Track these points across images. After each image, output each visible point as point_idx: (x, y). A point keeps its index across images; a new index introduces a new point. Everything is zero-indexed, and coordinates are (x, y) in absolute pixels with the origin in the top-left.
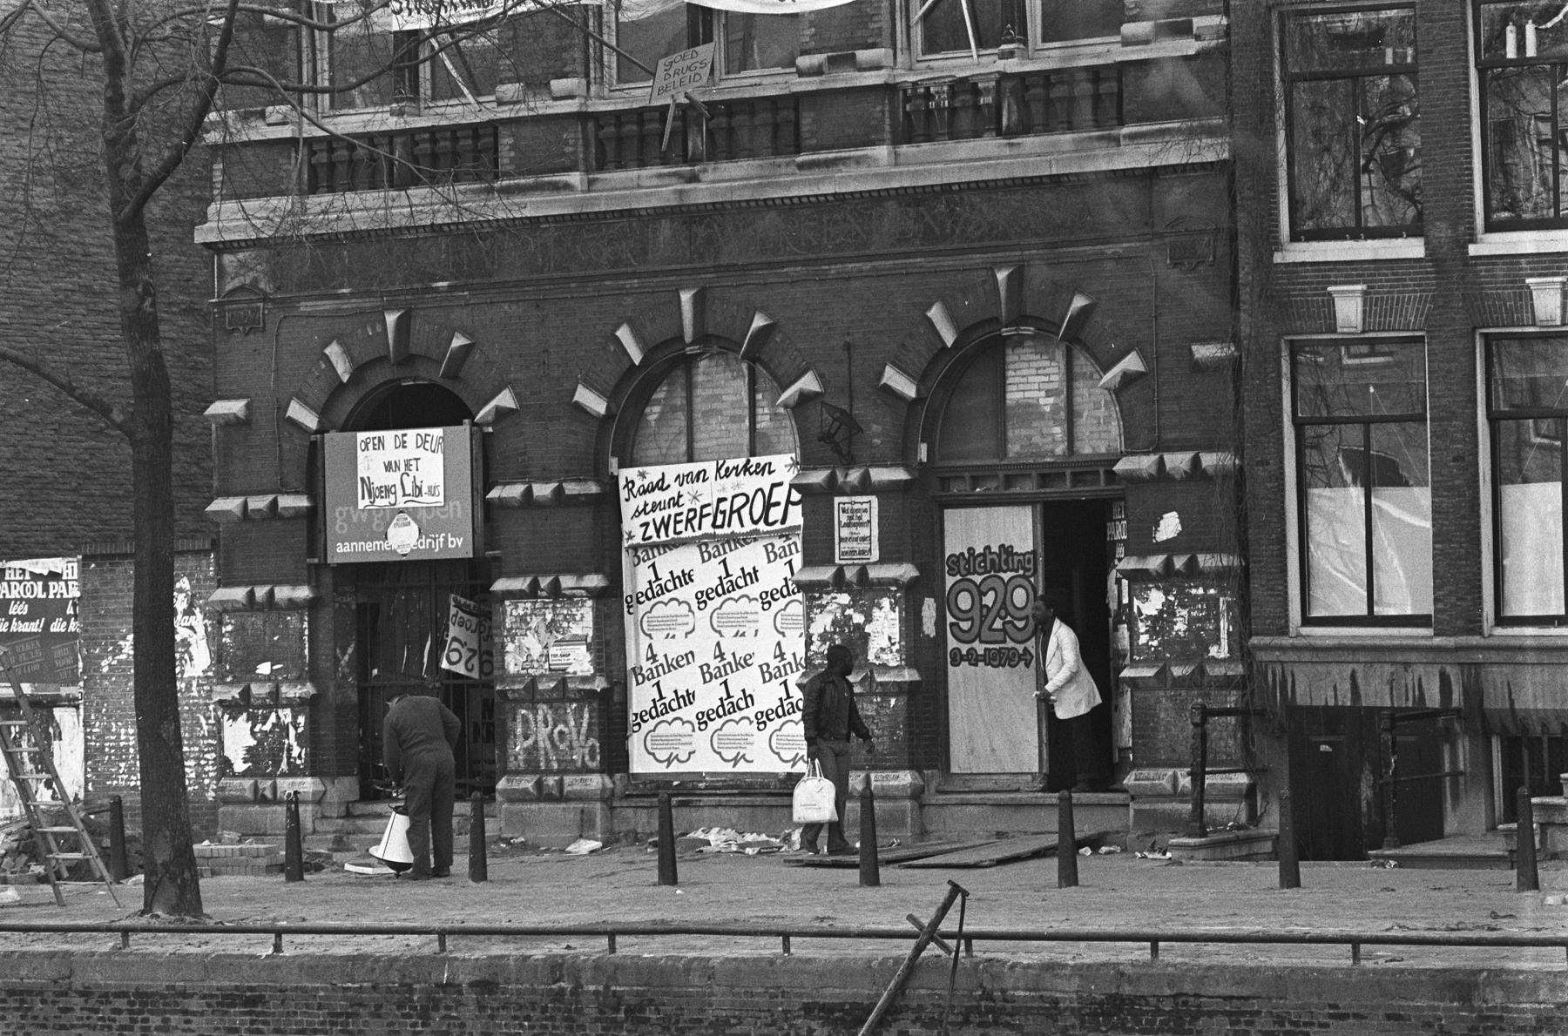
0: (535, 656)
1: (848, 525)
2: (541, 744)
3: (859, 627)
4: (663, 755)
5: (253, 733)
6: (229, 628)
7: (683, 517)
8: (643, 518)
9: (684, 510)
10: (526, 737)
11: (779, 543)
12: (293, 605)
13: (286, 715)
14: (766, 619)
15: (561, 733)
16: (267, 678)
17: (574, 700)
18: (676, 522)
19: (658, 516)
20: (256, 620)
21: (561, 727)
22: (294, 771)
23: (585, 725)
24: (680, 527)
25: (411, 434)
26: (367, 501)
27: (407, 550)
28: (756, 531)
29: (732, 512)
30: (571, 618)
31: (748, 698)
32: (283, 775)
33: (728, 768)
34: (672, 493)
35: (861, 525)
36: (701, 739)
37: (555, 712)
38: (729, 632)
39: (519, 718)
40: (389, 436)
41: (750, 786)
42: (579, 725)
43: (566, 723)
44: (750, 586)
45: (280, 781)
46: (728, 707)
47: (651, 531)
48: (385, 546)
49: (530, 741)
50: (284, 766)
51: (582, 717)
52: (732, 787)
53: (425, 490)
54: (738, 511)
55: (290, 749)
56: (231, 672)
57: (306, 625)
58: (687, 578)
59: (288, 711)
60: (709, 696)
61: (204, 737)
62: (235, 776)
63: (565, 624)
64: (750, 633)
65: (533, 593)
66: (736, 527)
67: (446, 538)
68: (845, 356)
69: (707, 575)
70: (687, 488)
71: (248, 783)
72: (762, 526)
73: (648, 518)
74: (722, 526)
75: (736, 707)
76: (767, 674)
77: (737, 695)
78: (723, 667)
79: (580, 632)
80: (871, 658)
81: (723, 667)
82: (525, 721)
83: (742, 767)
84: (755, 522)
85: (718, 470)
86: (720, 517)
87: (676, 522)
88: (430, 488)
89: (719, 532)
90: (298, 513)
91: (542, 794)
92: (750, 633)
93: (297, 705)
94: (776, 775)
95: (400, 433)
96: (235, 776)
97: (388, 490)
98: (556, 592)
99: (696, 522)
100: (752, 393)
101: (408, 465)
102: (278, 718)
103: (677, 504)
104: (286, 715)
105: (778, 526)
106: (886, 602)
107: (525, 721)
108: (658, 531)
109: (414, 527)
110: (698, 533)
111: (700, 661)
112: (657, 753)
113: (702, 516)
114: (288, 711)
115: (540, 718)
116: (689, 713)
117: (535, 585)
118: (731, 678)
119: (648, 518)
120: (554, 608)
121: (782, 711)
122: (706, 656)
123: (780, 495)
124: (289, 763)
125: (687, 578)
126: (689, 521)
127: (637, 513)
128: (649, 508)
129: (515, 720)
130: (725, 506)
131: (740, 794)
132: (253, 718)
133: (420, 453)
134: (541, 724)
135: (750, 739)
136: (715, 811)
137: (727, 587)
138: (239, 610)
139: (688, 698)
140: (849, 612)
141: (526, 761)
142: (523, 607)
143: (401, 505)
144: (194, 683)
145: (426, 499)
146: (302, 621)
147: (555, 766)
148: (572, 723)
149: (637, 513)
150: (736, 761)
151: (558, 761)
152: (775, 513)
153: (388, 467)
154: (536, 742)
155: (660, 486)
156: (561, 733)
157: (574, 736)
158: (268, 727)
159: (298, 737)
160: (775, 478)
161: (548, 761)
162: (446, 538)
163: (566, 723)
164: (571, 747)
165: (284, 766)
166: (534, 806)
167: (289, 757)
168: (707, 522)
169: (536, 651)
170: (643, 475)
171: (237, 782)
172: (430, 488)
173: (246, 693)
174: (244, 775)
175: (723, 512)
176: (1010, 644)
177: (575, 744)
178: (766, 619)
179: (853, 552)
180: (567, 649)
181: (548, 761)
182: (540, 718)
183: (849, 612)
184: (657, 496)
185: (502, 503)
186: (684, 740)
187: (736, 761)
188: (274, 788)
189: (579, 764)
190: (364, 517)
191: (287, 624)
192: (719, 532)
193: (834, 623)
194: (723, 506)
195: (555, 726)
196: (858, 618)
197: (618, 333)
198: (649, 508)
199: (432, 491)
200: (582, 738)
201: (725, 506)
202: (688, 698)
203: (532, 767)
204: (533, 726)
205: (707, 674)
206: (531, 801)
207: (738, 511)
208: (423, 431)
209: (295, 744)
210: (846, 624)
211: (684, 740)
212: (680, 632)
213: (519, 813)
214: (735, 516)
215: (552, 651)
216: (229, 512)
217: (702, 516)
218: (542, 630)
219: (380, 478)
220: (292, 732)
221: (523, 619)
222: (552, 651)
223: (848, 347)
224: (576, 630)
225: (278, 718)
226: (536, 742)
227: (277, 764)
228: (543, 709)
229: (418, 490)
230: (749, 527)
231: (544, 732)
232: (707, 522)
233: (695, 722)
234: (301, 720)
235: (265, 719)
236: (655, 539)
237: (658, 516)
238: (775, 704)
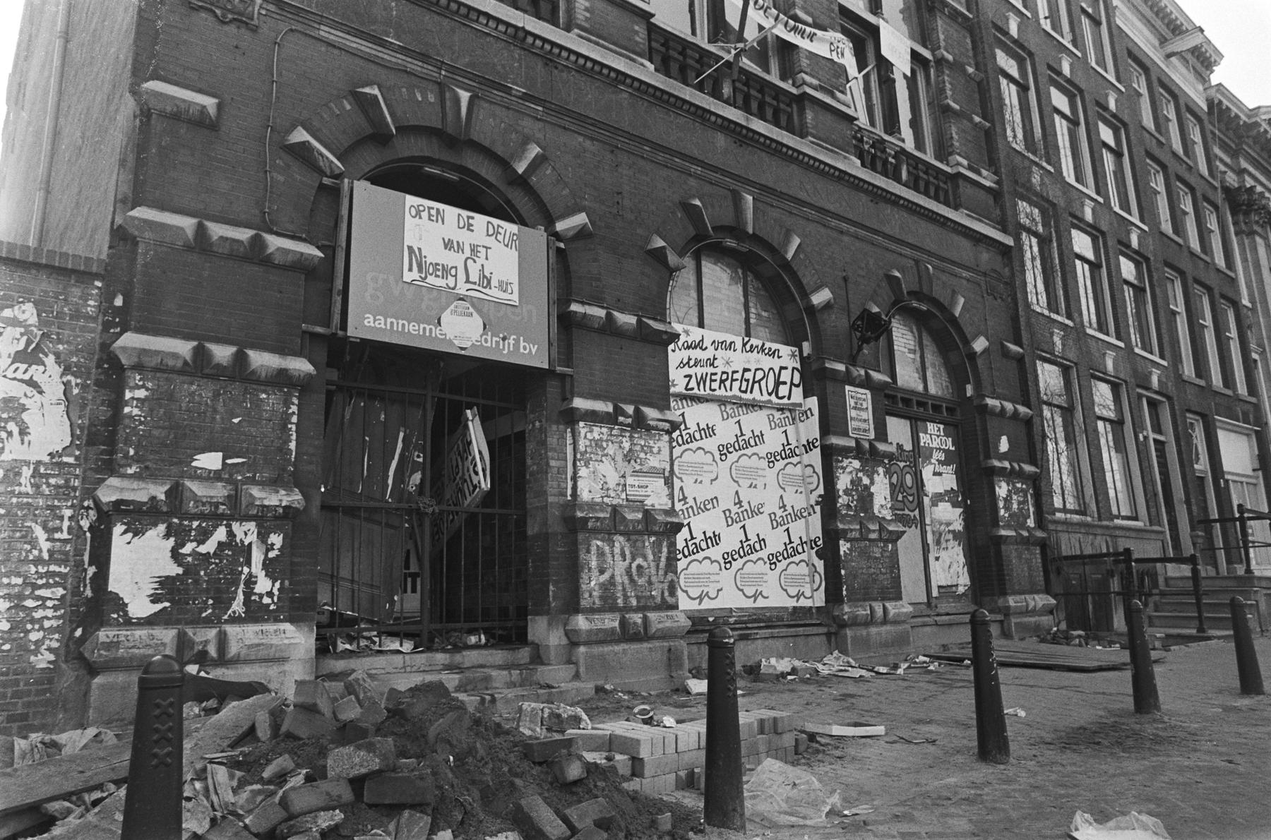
0: (612, 485)
1: (855, 408)
2: (618, 579)
3: (867, 488)
4: (793, 591)
5: (176, 555)
6: (141, 394)
7: (718, 377)
8: (687, 371)
9: (719, 371)
10: (602, 572)
11: (777, 415)
12: (281, 380)
13: (246, 532)
14: (771, 474)
15: (639, 567)
16: (215, 476)
17: (655, 534)
18: (712, 380)
19: (699, 371)
20: (203, 391)
21: (639, 561)
22: (256, 612)
23: (663, 559)
24: (715, 385)
25: (480, 220)
26: (415, 275)
27: (467, 344)
28: (770, 401)
29: (754, 382)
30: (648, 450)
31: (762, 541)
32: (235, 620)
33: (749, 604)
34: (710, 353)
35: (862, 410)
36: (726, 577)
37: (633, 546)
38: (745, 483)
39: (594, 549)
40: (451, 212)
41: (770, 619)
42: (657, 560)
43: (645, 558)
44: (759, 446)
45: (231, 630)
46: (748, 548)
47: (693, 384)
48: (436, 332)
49: (606, 576)
50: (238, 606)
51: (660, 552)
52: (755, 621)
53: (494, 283)
54: (759, 381)
55: (251, 581)
56: (137, 459)
57: (294, 409)
58: (709, 431)
59: (252, 526)
60: (731, 539)
61: (38, 561)
62: (128, 622)
63: (642, 455)
64: (760, 486)
65: (608, 420)
66: (756, 395)
67: (517, 341)
68: (842, 284)
69: (726, 432)
70: (720, 353)
71: (167, 635)
72: (773, 397)
73: (691, 371)
74: (745, 392)
75: (753, 550)
76: (775, 523)
77: (753, 539)
78: (741, 513)
79: (657, 465)
80: (876, 511)
81: (741, 513)
82: (601, 554)
83: (761, 603)
84: (770, 394)
85: (744, 345)
86: (744, 384)
87: (712, 380)
88: (501, 282)
89: (744, 396)
90: (300, 266)
91: (628, 634)
92: (760, 486)
93: (266, 520)
94: (787, 608)
95: (465, 213)
96: (128, 622)
97: (446, 271)
98: (639, 423)
99: (728, 383)
100: (746, 295)
101: (474, 249)
102: (231, 534)
103: (712, 365)
104: (246, 532)
105: (785, 401)
106: (881, 470)
107: (601, 554)
108: (698, 384)
109: (477, 321)
110: (729, 394)
111: (723, 506)
112: (690, 590)
113: (733, 380)
114: (252, 526)
115: (617, 550)
116: (716, 553)
117: (618, 411)
118: (748, 523)
119: (691, 371)
120: (631, 437)
121: (790, 551)
122: (727, 502)
123: (785, 376)
124: (247, 602)
125: (709, 431)
126: (722, 381)
127: (682, 365)
128: (692, 363)
129: (588, 551)
130: (749, 375)
131: (767, 627)
132: (178, 535)
133: (490, 241)
134: (618, 558)
135: (765, 578)
136: (767, 643)
137: (742, 444)
138: (173, 371)
139: (715, 539)
140: (860, 475)
141: (601, 597)
142: (599, 432)
143: (462, 289)
144: (27, 472)
145: (495, 293)
146: (287, 404)
147: (634, 602)
148: (651, 557)
149: (682, 365)
150: (755, 597)
151: (638, 598)
152: (783, 390)
153: (448, 245)
154: (612, 577)
155: (699, 345)
156: (639, 567)
157: (653, 571)
158: (209, 547)
159: (268, 565)
160: (783, 362)
161: (626, 597)
162: (517, 341)
163: (645, 558)
164: (650, 583)
165: (238, 606)
166: (618, 648)
167: (248, 593)
168: (736, 385)
169: (613, 479)
170: (687, 332)
171: (140, 633)
172: (501, 282)
173: (175, 493)
174: (150, 621)
175: (747, 381)
176: (906, 512)
177: (654, 579)
178: (771, 474)
179: (859, 429)
180: (644, 480)
181: (626, 597)
182: (617, 550)
183: (860, 475)
184: (696, 354)
185: (583, 323)
186: (713, 578)
187: (755, 597)
188: (222, 640)
189: (659, 600)
190: (409, 293)
191: (258, 404)
192: (744, 396)
193: (852, 482)
194: (747, 375)
195: (633, 559)
196: (866, 481)
197: (584, 214)
198: (692, 363)
199: (503, 286)
200: (661, 572)
201: (749, 375)
202: (715, 539)
203: (608, 604)
204: (609, 559)
205: (730, 519)
206: (618, 641)
207: (759, 381)
208: (496, 221)
209: (261, 575)
210: (859, 485)
211: (713, 578)
212: (706, 481)
213: (602, 657)
214: (756, 385)
215: (630, 481)
216: (182, 229)
217: (733, 380)
218: (619, 458)
219: (435, 254)
220: (257, 556)
221: (598, 444)
222: (630, 481)
223: (845, 279)
224: (653, 462)
225: (231, 534)
226: (612, 577)
227: (223, 602)
228: (619, 540)
229: (486, 281)
230: (766, 397)
231: (620, 566)
232: (736, 385)
233: (722, 561)
234: (276, 539)
235: (203, 536)
236: (696, 391)
237: (699, 371)
238: (737, 546)
